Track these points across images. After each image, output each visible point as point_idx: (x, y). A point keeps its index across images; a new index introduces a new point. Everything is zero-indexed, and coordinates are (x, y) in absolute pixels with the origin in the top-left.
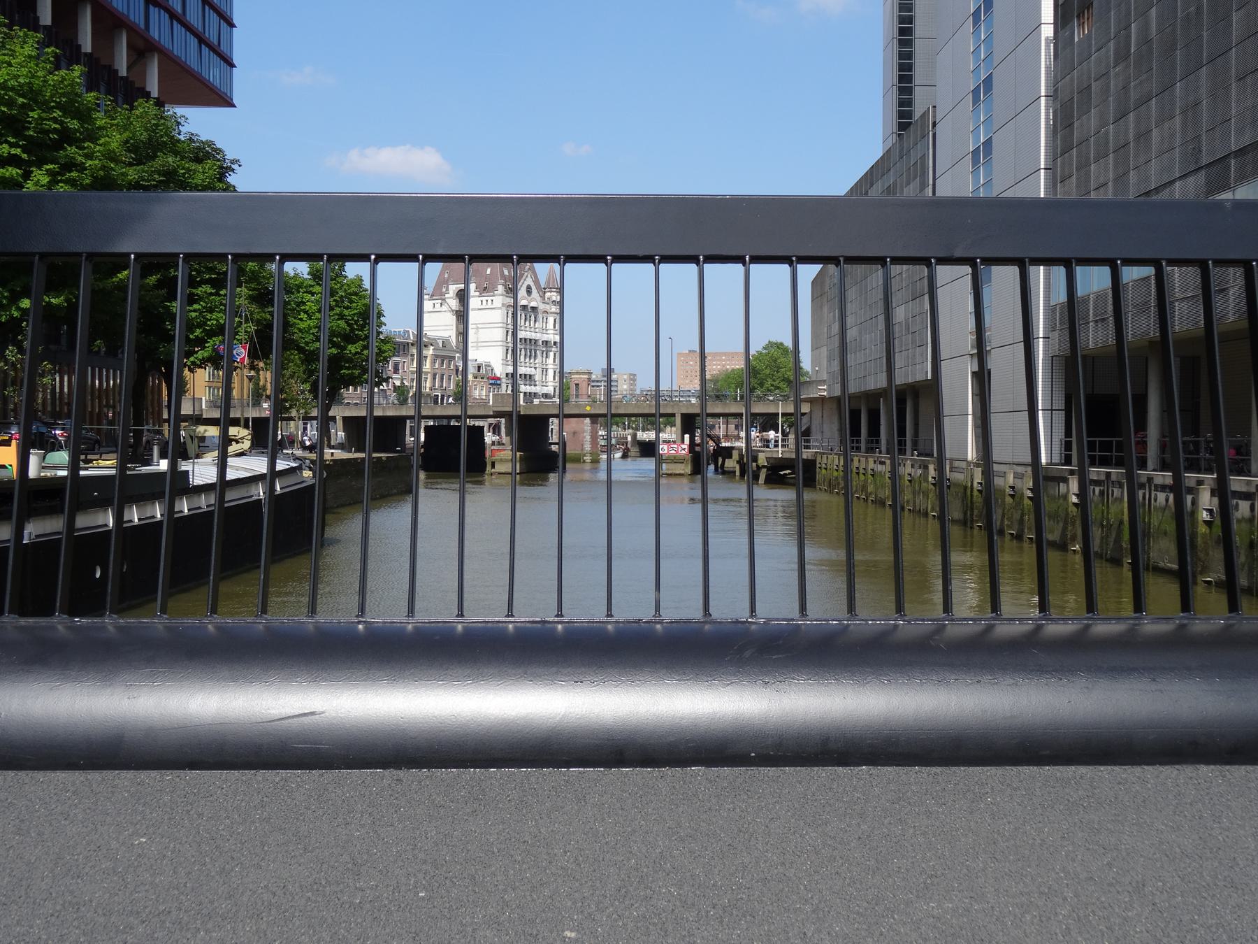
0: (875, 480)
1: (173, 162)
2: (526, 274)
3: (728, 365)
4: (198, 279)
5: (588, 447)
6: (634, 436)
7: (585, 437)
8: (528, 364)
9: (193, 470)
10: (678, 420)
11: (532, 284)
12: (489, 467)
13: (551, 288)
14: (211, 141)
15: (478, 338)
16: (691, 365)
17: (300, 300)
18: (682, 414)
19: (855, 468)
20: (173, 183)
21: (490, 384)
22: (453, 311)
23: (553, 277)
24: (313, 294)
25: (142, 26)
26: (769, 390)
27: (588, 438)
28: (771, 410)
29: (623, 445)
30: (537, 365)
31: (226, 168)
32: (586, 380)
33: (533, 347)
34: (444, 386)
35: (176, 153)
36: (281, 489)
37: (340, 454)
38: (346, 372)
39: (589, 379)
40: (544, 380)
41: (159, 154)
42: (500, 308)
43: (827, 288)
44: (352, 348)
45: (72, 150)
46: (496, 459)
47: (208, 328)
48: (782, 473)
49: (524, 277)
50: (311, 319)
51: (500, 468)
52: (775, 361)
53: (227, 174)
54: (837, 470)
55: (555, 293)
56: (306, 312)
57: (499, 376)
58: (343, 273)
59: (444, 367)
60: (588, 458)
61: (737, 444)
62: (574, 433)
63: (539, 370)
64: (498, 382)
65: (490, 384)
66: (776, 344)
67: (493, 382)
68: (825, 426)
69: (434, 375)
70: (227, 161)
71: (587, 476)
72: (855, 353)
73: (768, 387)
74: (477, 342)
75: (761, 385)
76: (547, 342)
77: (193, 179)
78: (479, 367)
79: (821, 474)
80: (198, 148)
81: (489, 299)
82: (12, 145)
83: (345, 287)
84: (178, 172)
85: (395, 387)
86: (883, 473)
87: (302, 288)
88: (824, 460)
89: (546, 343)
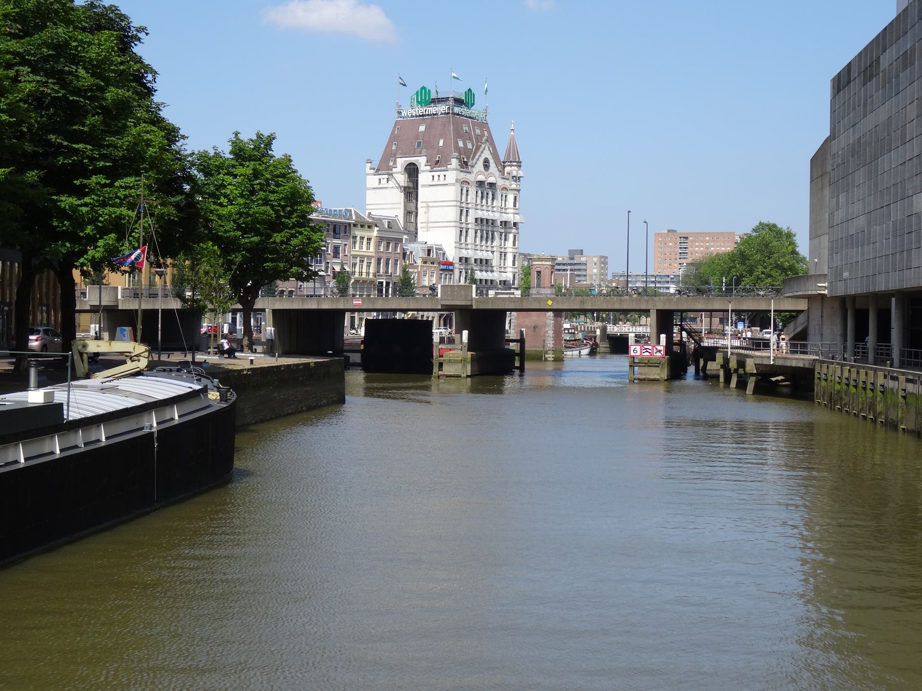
0: (885, 399)
1: (64, 33)
2: (483, 146)
3: (712, 246)
4: (91, 168)
5: (550, 343)
6: (604, 329)
7: (547, 332)
8: (484, 248)
9: (68, 403)
10: (653, 314)
11: (490, 157)
12: (435, 369)
13: (511, 162)
14: (114, 6)
15: (428, 218)
16: (670, 247)
17: (220, 182)
18: (657, 310)
19: (861, 383)
20: (64, 57)
21: (442, 270)
22: (401, 187)
23: (514, 149)
24: (235, 176)
26: (759, 278)
27: (551, 333)
28: (762, 306)
29: (591, 339)
30: (495, 249)
31: (132, 37)
32: (549, 267)
33: (490, 229)
34: (390, 271)
35: (68, 23)
36: (179, 417)
37: (262, 360)
39: (553, 267)
40: (502, 265)
41: (48, 24)
42: (453, 185)
43: (829, 169)
44: (278, 237)
46: (444, 360)
47: (100, 225)
48: (773, 379)
49: (481, 149)
50: (232, 204)
51: (448, 370)
52: (767, 246)
53: (133, 44)
54: (839, 383)
55: (516, 168)
56: (226, 196)
57: (451, 261)
58: (270, 152)
59: (390, 251)
60: (550, 356)
61: (721, 342)
62: (535, 327)
63: (497, 255)
64: (451, 268)
65: (442, 270)
66: (767, 225)
67: (445, 267)
68: (825, 327)
69: (379, 260)
70: (132, 29)
71: (549, 381)
72: (862, 246)
73: (758, 276)
74: (428, 223)
75: (751, 272)
76: (506, 222)
77: (87, 52)
78: (429, 251)
79: (820, 386)
80: (102, 15)
81: (442, 174)
83: (271, 168)
84: (70, 44)
85: (334, 273)
86: (895, 391)
87: (223, 169)
88: (824, 370)
89: (505, 224)
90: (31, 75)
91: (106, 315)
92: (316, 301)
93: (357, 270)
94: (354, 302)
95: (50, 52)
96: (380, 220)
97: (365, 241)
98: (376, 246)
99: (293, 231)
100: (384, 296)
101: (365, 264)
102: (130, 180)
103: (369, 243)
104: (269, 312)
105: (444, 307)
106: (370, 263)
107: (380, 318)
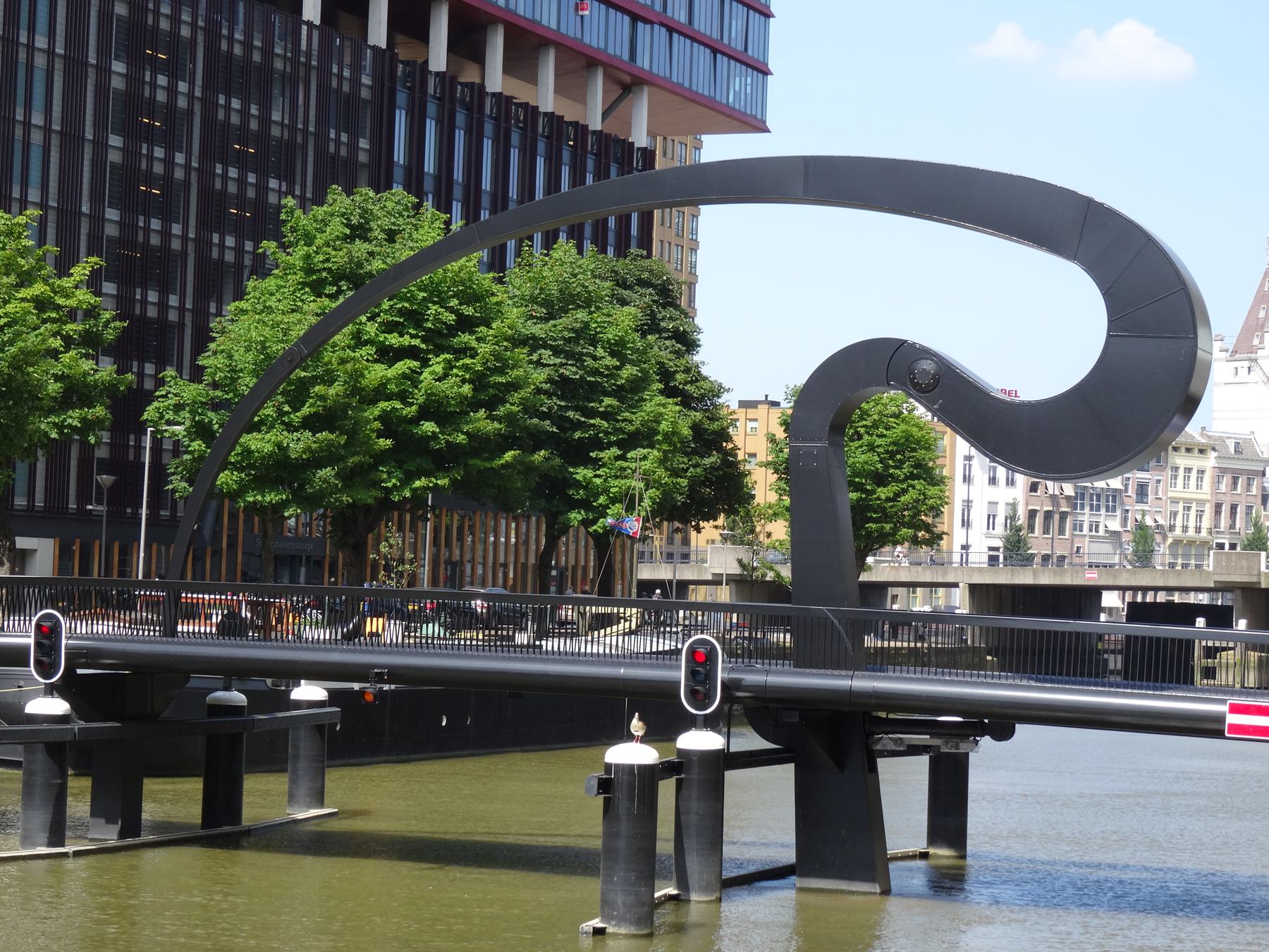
25: (626, 57)
34: (1238, 526)
38: (874, 526)
44: (883, 492)
45: (465, 338)
69: (1234, 508)
82: (412, 336)
90: (552, 357)
91: (734, 587)
92: (1031, 573)
93: (1179, 522)
94: (1087, 575)
95: (571, 335)
96: (1222, 439)
97: (1194, 475)
98: (1213, 483)
99: (905, 486)
100: (1001, 566)
101: (1193, 513)
102: (641, 451)
103: (1187, 478)
104: (964, 588)
105: (1218, 585)
106: (1202, 511)
107: (1219, 603)
